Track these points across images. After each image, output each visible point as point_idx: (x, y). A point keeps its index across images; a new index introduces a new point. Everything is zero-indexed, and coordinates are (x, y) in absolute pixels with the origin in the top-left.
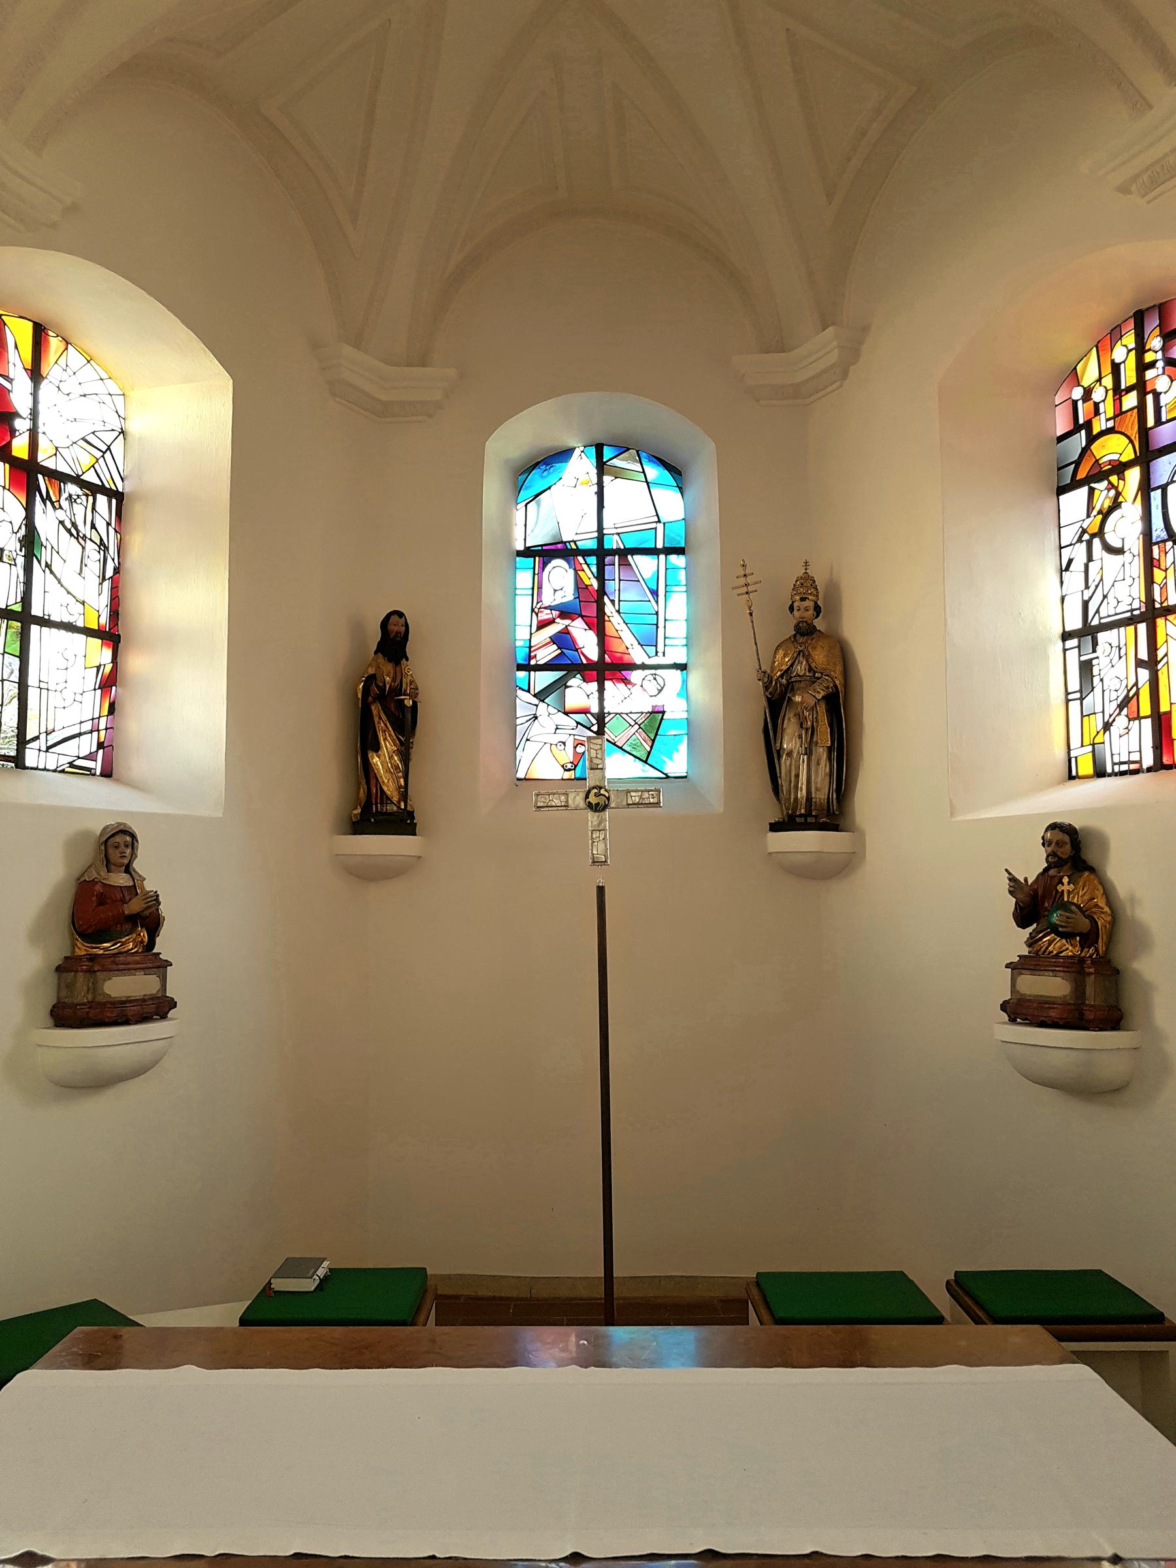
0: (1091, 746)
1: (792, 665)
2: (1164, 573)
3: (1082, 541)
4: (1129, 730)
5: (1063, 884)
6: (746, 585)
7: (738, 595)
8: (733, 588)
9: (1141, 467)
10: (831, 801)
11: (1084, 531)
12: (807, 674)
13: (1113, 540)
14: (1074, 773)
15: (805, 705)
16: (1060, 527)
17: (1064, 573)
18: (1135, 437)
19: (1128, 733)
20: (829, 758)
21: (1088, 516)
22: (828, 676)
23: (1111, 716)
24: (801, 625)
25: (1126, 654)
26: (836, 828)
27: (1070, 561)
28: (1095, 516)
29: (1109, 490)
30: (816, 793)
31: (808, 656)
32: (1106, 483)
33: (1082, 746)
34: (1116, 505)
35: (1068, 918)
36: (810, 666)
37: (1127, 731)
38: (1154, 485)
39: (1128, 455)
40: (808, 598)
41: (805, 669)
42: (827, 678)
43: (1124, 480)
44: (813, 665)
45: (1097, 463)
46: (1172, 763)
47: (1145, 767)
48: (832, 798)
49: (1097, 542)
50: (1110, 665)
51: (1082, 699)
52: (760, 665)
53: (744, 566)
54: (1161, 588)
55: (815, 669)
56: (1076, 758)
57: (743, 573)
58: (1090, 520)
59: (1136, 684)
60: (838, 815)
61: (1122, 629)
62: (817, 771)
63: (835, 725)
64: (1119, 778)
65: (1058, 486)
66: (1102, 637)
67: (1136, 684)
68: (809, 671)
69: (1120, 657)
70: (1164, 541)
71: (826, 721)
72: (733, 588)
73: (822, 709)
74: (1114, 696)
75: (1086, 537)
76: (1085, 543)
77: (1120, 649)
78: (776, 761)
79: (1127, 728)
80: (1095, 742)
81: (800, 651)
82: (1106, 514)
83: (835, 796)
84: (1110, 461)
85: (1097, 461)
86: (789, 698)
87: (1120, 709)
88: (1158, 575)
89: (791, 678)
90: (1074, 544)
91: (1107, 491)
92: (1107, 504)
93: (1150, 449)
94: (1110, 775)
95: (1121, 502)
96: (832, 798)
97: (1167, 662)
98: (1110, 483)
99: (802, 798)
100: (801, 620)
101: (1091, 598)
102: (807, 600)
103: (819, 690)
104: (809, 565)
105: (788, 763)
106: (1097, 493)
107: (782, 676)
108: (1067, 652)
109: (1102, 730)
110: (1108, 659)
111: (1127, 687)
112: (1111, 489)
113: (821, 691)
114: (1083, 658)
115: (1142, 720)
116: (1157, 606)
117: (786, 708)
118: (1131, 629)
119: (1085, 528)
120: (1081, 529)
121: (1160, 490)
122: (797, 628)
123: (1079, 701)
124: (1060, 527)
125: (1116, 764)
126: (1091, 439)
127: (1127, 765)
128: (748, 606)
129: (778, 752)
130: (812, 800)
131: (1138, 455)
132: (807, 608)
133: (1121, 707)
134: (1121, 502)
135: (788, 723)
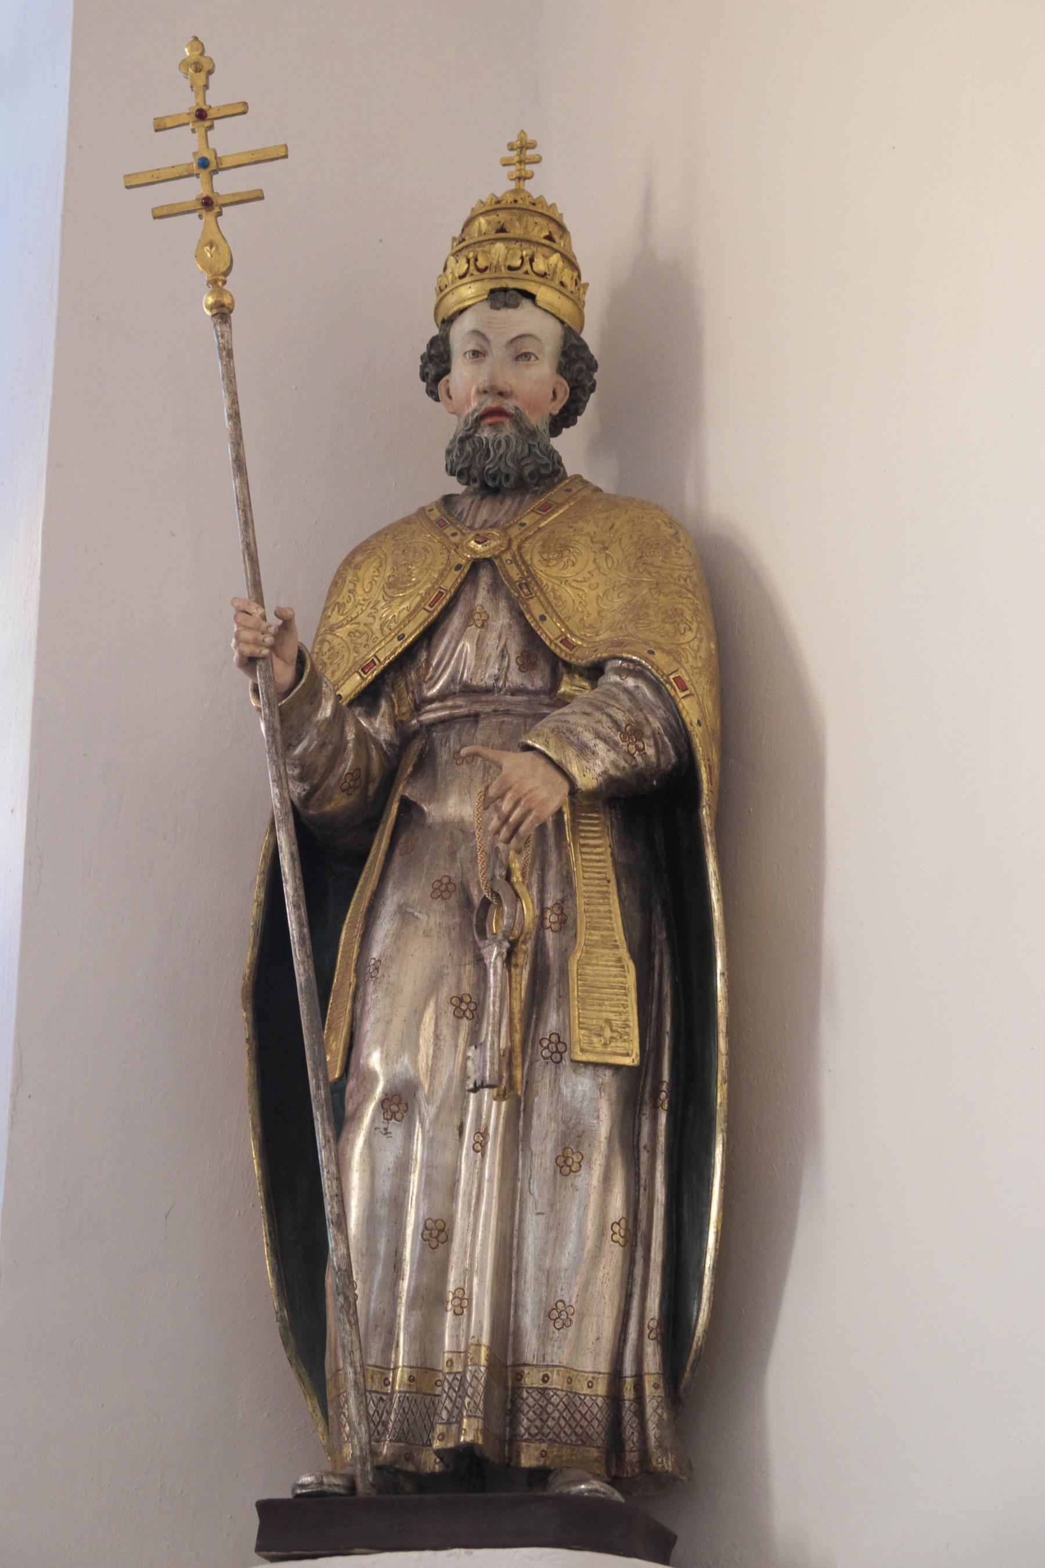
1: (429, 635)
6: (204, 163)
15: (506, 806)
22: (638, 671)
30: (544, 1338)
31: (524, 584)
40: (531, 297)
41: (503, 655)
42: (630, 682)
44: (550, 632)
52: (256, 584)
55: (563, 652)
57: (189, 103)
62: (555, 1228)
63: (663, 961)
68: (527, 663)
81: (476, 565)
83: (652, 1362)
86: (408, 806)
89: (419, 706)
99: (464, 1354)
102: (526, 303)
104: (537, 161)
105: (388, 1158)
113: (601, 748)
128: (208, 267)
129: (337, 1091)
130: (519, 1377)
135: (397, 936)
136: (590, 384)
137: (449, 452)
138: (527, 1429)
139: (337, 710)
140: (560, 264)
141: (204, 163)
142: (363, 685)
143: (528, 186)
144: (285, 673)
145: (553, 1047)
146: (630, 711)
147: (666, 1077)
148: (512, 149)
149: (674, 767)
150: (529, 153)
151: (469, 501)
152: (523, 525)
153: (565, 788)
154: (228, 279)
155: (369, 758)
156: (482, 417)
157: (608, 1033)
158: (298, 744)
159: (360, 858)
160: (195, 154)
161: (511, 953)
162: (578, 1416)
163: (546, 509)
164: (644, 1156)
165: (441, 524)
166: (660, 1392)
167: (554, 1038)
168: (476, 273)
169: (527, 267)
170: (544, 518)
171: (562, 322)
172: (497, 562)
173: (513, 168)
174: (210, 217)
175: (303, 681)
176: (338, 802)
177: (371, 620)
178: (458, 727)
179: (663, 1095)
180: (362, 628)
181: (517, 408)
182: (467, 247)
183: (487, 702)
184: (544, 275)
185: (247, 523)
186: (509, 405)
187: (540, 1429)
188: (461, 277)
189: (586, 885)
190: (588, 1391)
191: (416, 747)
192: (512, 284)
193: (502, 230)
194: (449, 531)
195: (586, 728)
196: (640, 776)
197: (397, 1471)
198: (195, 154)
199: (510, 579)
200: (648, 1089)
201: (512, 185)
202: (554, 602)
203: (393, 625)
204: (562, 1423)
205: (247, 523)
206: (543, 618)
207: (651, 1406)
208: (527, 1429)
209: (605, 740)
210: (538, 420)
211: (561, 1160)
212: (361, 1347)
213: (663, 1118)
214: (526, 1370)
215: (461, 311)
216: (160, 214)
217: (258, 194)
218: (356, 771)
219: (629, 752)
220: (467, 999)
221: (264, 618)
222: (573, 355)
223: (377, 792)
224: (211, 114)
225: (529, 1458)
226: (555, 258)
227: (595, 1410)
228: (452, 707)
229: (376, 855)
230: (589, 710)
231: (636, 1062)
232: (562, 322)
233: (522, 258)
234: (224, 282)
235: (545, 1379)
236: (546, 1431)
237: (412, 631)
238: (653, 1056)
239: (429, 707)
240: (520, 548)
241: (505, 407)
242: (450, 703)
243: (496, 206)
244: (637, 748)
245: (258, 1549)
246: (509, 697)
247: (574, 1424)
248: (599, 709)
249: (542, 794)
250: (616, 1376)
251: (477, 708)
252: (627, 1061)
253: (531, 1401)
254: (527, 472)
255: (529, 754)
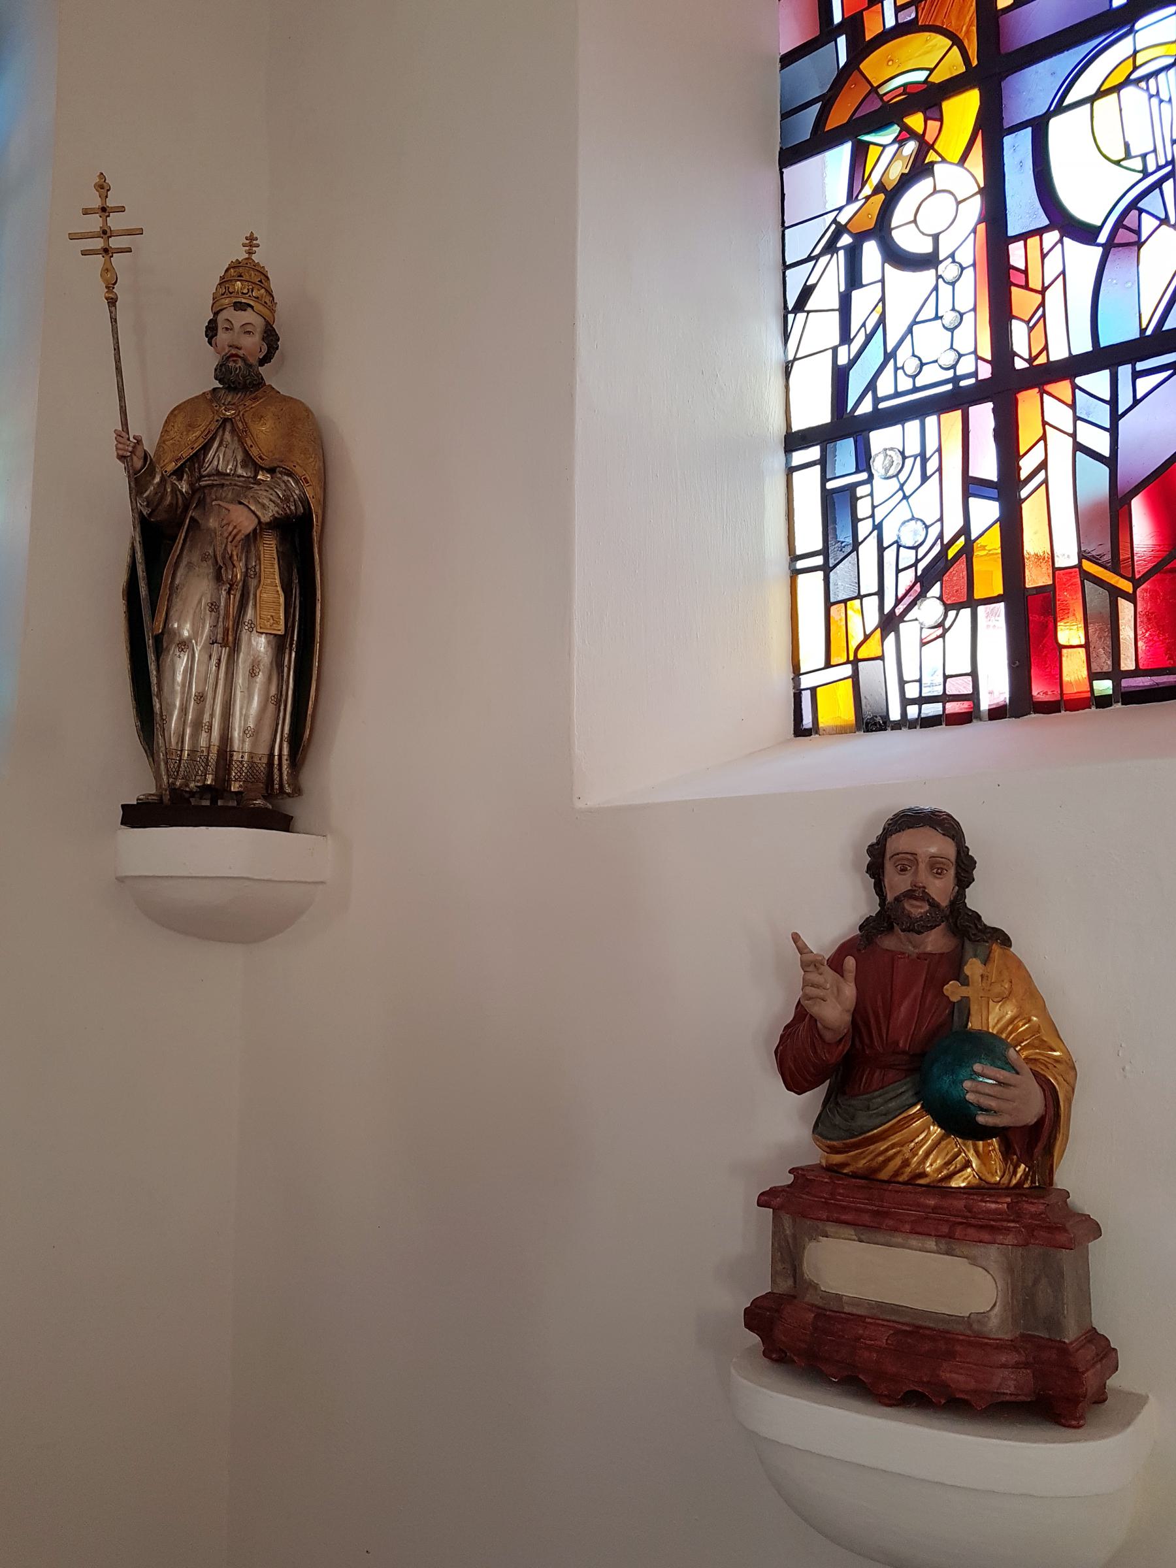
0: (849, 666)
2: (1040, 297)
3: (837, 250)
4: (946, 631)
5: (965, 982)
6: (104, 232)
7: (84, 253)
8: (73, 237)
9: (980, 90)
10: (276, 762)
11: (840, 230)
12: (240, 471)
13: (908, 240)
14: (807, 722)
16: (784, 228)
17: (791, 317)
18: (968, 32)
19: (942, 636)
20: (278, 663)
21: (851, 198)
23: (898, 601)
24: (231, 364)
25: (940, 469)
26: (284, 823)
27: (807, 292)
28: (867, 198)
29: (900, 141)
32: (895, 130)
33: (828, 665)
34: (920, 169)
35: (1000, 1083)
36: (246, 453)
37: (939, 631)
38: (1008, 123)
39: (954, 65)
43: (941, 120)
44: (254, 452)
45: (873, 95)
46: (1059, 698)
47: (984, 706)
48: (280, 756)
49: (871, 251)
50: (900, 494)
51: (826, 569)
52: (125, 424)
53: (102, 188)
54: (1031, 329)
55: (259, 462)
56: (813, 690)
57: (97, 203)
58: (855, 206)
59: (965, 530)
60: (288, 794)
61: (931, 421)
63: (296, 591)
64: (919, 734)
65: (781, 148)
66: (880, 439)
67: (965, 530)
69: (925, 478)
70: (1039, 232)
71: (277, 577)
72: (73, 237)
73: (269, 548)
74: (907, 557)
75: (846, 240)
76: (841, 253)
77: (925, 462)
78: (151, 657)
79: (941, 624)
80: (860, 656)
81: (226, 420)
82: (892, 195)
83: (285, 751)
84: (905, 86)
85: (875, 90)
87: (922, 586)
88: (1022, 301)
90: (817, 258)
91: (896, 146)
92: (898, 170)
93: (1003, 52)
94: (897, 726)
95: (932, 163)
96: (280, 756)
97: (1045, 482)
98: (905, 128)
100: (234, 351)
101: (852, 362)
102: (249, 309)
103: (266, 502)
104: (258, 246)
106: (873, 152)
107: (179, 473)
108: (796, 475)
109: (878, 632)
110: (894, 484)
111: (941, 536)
112: (907, 140)
114: (830, 485)
115: (981, 610)
116: (1020, 364)
117: (185, 540)
118: (953, 419)
119: (843, 222)
120: (833, 226)
121: (1029, 130)
122: (222, 372)
123: (820, 574)
124: (784, 228)
125: (913, 702)
126: (860, 49)
127: (940, 705)
128: (105, 280)
129: (158, 639)
130: (232, 756)
131: (975, 63)
132: (249, 328)
133: (925, 581)
134: (932, 163)
136: (275, 346)
137: (216, 370)
138: (234, 776)
139: (163, 479)
140: (265, 293)
141: (104, 232)
142: (176, 467)
143: (254, 257)
144: (138, 464)
145: (249, 626)
146: (285, 491)
147: (295, 639)
148: (247, 239)
149: (303, 513)
150: (255, 242)
151: (223, 392)
152: (245, 405)
153: (256, 521)
154: (115, 286)
155: (177, 499)
156: (229, 357)
157: (272, 621)
158: (145, 492)
159: (174, 538)
160: (101, 228)
161: (230, 589)
162: (255, 771)
163: (255, 399)
164: (286, 669)
165: (211, 401)
166: (288, 762)
167: (250, 622)
168: (229, 294)
169: (250, 293)
170: (254, 403)
171: (265, 319)
172: (233, 420)
173: (247, 248)
174: (107, 257)
175: (148, 463)
176: (161, 516)
177: (180, 439)
178: (215, 489)
179: (294, 646)
180: (177, 443)
181: (244, 354)
182: (225, 282)
183: (227, 480)
184: (257, 298)
185: (122, 397)
186: (241, 353)
187: (239, 777)
188: (223, 295)
189: (272, 547)
190: (260, 761)
191: (197, 496)
192: (243, 301)
193: (241, 276)
194: (214, 405)
195: (266, 497)
196: (287, 517)
197: (183, 790)
198: (101, 228)
199: (238, 428)
200: (288, 643)
201: (247, 256)
202: (256, 440)
203: (189, 443)
204: (248, 774)
205: (122, 397)
206: (251, 446)
207: (285, 767)
208: (234, 776)
209: (274, 502)
210: (253, 361)
211: (251, 671)
212: (184, 725)
213: (293, 655)
214: (235, 753)
215: (221, 310)
216: (85, 253)
217: (129, 250)
218: (170, 505)
219: (284, 508)
220: (215, 604)
221: (129, 439)
222: (269, 333)
223: (181, 513)
224: (108, 210)
225: (235, 787)
226: (263, 291)
227: (262, 769)
228: (213, 480)
229: (179, 540)
230: (268, 489)
231: (283, 633)
232: (265, 319)
233: (248, 289)
234: (113, 288)
235: (242, 757)
236: (242, 777)
237: (197, 446)
238: (290, 629)
239: (203, 479)
240: (243, 415)
241: (239, 354)
242: (212, 478)
243: (235, 265)
244: (287, 506)
245: (122, 824)
246: (236, 478)
247: (253, 774)
248: (272, 489)
249: (246, 523)
250: (271, 755)
251: (223, 481)
252: (279, 633)
253: (236, 766)
254: (248, 381)
255: (242, 506)
